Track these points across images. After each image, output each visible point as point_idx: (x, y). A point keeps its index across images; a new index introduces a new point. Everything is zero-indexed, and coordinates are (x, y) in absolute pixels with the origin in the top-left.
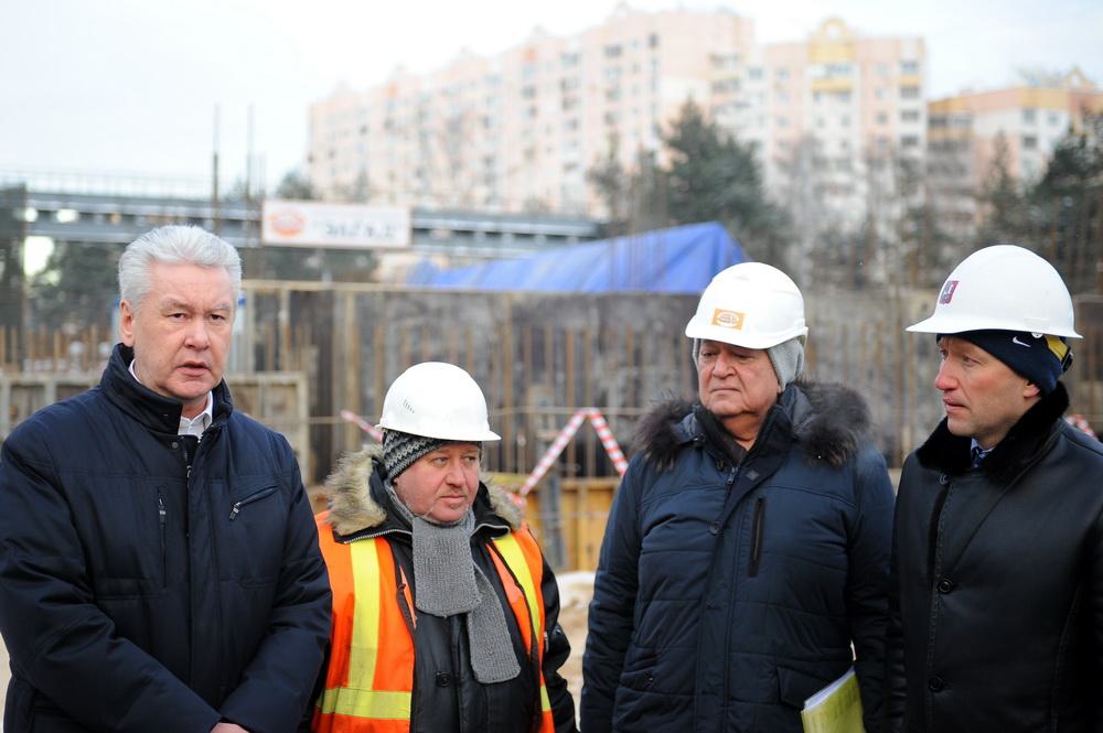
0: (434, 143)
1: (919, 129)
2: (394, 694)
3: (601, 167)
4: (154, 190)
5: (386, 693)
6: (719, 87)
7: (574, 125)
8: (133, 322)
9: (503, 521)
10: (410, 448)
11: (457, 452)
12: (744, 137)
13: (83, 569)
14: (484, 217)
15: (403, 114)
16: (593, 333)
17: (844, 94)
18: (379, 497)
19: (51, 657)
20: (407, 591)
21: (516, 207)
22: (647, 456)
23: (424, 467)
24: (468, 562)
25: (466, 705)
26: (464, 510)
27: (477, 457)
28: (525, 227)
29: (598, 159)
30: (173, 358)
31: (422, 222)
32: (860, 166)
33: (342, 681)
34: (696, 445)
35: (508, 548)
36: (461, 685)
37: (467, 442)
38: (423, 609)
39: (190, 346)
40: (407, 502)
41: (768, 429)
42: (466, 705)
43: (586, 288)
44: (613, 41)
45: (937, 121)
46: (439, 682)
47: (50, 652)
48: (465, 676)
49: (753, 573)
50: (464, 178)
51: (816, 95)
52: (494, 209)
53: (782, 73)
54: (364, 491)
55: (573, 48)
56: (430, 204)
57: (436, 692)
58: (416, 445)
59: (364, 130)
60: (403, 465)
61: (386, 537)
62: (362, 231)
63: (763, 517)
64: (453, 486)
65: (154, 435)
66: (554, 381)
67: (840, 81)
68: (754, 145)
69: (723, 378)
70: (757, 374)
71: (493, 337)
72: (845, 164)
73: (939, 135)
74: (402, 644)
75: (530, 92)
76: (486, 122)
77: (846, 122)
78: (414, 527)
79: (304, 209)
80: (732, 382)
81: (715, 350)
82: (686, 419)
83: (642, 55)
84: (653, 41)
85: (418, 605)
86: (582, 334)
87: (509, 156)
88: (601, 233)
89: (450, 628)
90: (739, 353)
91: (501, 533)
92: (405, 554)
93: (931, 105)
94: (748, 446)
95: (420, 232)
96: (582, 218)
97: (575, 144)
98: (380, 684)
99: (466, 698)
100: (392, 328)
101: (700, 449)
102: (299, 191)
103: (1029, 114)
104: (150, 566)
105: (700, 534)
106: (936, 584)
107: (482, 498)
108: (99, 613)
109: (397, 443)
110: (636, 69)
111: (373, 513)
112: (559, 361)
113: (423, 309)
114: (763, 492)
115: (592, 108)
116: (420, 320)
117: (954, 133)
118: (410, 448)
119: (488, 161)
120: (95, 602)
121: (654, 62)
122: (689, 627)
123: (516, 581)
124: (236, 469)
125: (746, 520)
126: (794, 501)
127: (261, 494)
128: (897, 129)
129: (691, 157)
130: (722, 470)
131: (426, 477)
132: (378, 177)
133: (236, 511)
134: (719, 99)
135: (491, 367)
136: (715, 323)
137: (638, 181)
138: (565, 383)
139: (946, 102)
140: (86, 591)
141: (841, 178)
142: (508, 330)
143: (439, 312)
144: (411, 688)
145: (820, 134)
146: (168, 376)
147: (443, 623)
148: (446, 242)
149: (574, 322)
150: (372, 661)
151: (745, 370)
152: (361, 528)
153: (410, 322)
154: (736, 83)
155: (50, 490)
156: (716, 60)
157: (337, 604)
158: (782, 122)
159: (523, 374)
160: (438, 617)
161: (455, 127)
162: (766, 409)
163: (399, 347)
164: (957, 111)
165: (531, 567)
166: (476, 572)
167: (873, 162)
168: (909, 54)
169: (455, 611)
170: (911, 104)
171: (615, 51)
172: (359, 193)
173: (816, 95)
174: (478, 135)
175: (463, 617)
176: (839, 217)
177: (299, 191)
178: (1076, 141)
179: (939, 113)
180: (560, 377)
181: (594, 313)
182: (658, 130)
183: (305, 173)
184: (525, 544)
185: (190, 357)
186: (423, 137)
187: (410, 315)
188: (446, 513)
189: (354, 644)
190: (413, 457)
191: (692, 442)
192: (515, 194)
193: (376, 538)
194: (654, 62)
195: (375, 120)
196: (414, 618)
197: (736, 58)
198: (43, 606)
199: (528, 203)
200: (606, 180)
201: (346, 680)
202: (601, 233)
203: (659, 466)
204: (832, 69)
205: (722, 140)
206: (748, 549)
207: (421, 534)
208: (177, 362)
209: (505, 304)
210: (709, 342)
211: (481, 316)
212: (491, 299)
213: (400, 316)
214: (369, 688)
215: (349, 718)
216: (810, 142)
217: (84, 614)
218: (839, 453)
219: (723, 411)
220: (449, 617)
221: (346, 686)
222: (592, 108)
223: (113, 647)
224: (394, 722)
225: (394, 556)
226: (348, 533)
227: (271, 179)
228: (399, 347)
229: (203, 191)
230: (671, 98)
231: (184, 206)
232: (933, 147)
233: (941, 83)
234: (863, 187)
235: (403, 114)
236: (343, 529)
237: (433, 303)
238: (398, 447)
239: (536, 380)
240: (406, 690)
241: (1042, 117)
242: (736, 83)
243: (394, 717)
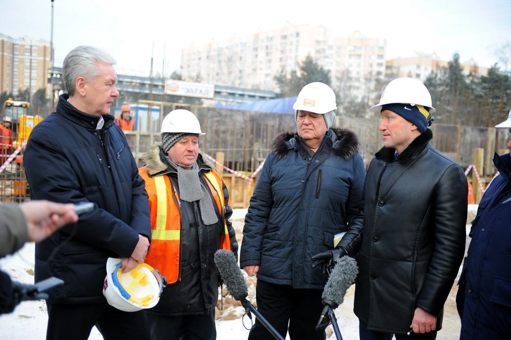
0: (223, 65)
1: (383, 69)
3: (278, 75)
4: (129, 73)
5: (171, 231)
6: (318, 51)
7: (270, 61)
10: (173, 139)
11: (190, 138)
12: (326, 68)
14: (238, 89)
15: (213, 54)
16: (277, 127)
17: (359, 56)
18: (164, 160)
20: (176, 194)
21: (249, 87)
22: (276, 153)
23: (178, 145)
24: (199, 183)
26: (193, 162)
27: (198, 142)
28: (252, 94)
29: (277, 72)
31: (218, 90)
32: (362, 80)
34: (295, 150)
35: (210, 176)
36: (199, 226)
37: (191, 133)
38: (183, 199)
40: (173, 159)
41: (323, 144)
43: (274, 111)
44: (285, 34)
45: (388, 67)
46: (191, 225)
48: (200, 223)
49: (317, 198)
50: (233, 76)
51: (350, 56)
52: (242, 87)
53: (339, 48)
54: (158, 158)
55: (271, 35)
56: (220, 84)
57: (190, 230)
58: (175, 137)
59: (200, 59)
60: (170, 145)
61: (167, 175)
62: (198, 92)
63: (321, 177)
64: (189, 151)
66: (263, 142)
67: (358, 52)
68: (329, 71)
69: (307, 125)
70: (320, 124)
71: (243, 125)
72: (358, 80)
73: (389, 72)
74: (175, 213)
75: (256, 49)
76: (241, 58)
77: (359, 65)
78: (178, 170)
79: (179, 83)
80: (310, 127)
81: (304, 114)
82: (291, 140)
83: (294, 39)
84: (298, 35)
85: (181, 198)
86: (273, 126)
87: (248, 70)
88: (278, 96)
89: (193, 206)
90: (313, 115)
91: (208, 171)
92: (175, 180)
93: (387, 62)
94: (315, 151)
95: (217, 93)
96: (271, 92)
97: (269, 68)
98: (168, 228)
100: (210, 121)
101: (296, 151)
102: (177, 77)
103: (418, 67)
105: (297, 183)
106: (378, 202)
107: (200, 159)
109: (168, 138)
110: (291, 44)
111: (162, 166)
112: (265, 135)
113: (220, 115)
114: (320, 168)
115: (276, 56)
116: (219, 119)
117: (395, 71)
118: (173, 139)
119: (241, 71)
121: (297, 42)
122: (295, 214)
123: (214, 188)
125: (315, 178)
126: (332, 169)
127: (329, 215)
128: (376, 69)
129: (308, 74)
130: (305, 159)
131: (179, 150)
132: (203, 74)
134: (318, 55)
135: (242, 136)
136: (304, 104)
137: (291, 80)
138: (267, 142)
139: (392, 61)
141: (357, 84)
142: (248, 123)
143: (226, 116)
144: (180, 228)
145: (351, 69)
147: (191, 204)
148: (225, 97)
149: (271, 122)
150: (165, 220)
151: (315, 122)
152: (158, 171)
153: (216, 119)
154: (324, 50)
155: (59, 156)
156: (318, 42)
157: (151, 199)
158: (338, 64)
159: (253, 138)
161: (230, 60)
162: (322, 137)
163: (211, 128)
164: (395, 64)
165: (219, 184)
166: (201, 186)
167: (368, 80)
168: (381, 44)
170: (380, 61)
171: (285, 37)
172: (198, 79)
173: (350, 56)
174: (238, 63)
175: (198, 202)
176: (356, 97)
177: (177, 77)
178: (434, 76)
179: (389, 64)
180: (265, 140)
181: (277, 119)
182: (297, 63)
183: (179, 72)
184: (216, 176)
186: (220, 62)
187: (216, 116)
188: (188, 162)
189: (158, 214)
190: (174, 142)
191: (293, 149)
192: (249, 82)
193: (164, 175)
194: (297, 42)
195: (204, 55)
196: (180, 203)
197: (325, 42)
199: (253, 86)
200: (280, 80)
201: (155, 227)
202: (278, 96)
203: (280, 157)
204: (355, 47)
205: (319, 68)
206: (315, 188)
207: (181, 172)
209: (248, 114)
210: (302, 111)
211: (239, 118)
212: (243, 113)
213: (212, 117)
215: (157, 241)
216: (348, 72)
218: (348, 155)
219: (307, 137)
220: (192, 202)
221: (155, 229)
222: (276, 56)
224: (174, 241)
225: (171, 182)
226: (154, 174)
227: (168, 73)
228: (211, 128)
229: (146, 74)
230: (302, 58)
231: (139, 79)
232: (387, 75)
233: (389, 56)
234: (363, 87)
235: (213, 54)
236: (152, 172)
237: (224, 113)
238: (169, 139)
239: (257, 141)
240: (178, 229)
241: (422, 67)
242: (324, 50)
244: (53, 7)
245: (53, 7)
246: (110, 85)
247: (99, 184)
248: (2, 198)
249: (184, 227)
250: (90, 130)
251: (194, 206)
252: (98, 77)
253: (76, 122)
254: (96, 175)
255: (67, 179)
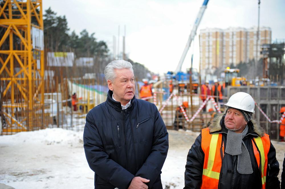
2: (216, 172)
8: (112, 85)
9: (256, 133)
13: (102, 144)
19: (94, 164)
25: (234, 178)
30: (125, 91)
33: (206, 168)
39: (129, 88)
42: (234, 178)
46: (228, 171)
47: (94, 162)
48: (235, 172)
57: (227, 174)
65: (116, 110)
91: (256, 137)
99: (234, 177)
104: (116, 143)
108: (105, 153)
120: (105, 151)
124: (138, 116)
133: (138, 126)
140: (102, 149)
146: (124, 96)
147: (232, 157)
150: (212, 164)
155: (93, 126)
160: (231, 155)
169: (235, 154)
175: (237, 156)
185: (129, 90)
198: (92, 152)
201: (207, 167)
208: (126, 92)
214: (211, 170)
217: (101, 154)
220: (234, 156)
221: (207, 169)
223: (107, 161)
240: (218, 172)
243: (215, 178)
244: (259, 7)
245: (259, 7)
246: (125, 81)
247: (113, 144)
248: (283, 105)
249: (223, 172)
250: (118, 110)
251: (234, 159)
252: (116, 78)
253: (111, 105)
254: (112, 139)
255: (94, 140)
